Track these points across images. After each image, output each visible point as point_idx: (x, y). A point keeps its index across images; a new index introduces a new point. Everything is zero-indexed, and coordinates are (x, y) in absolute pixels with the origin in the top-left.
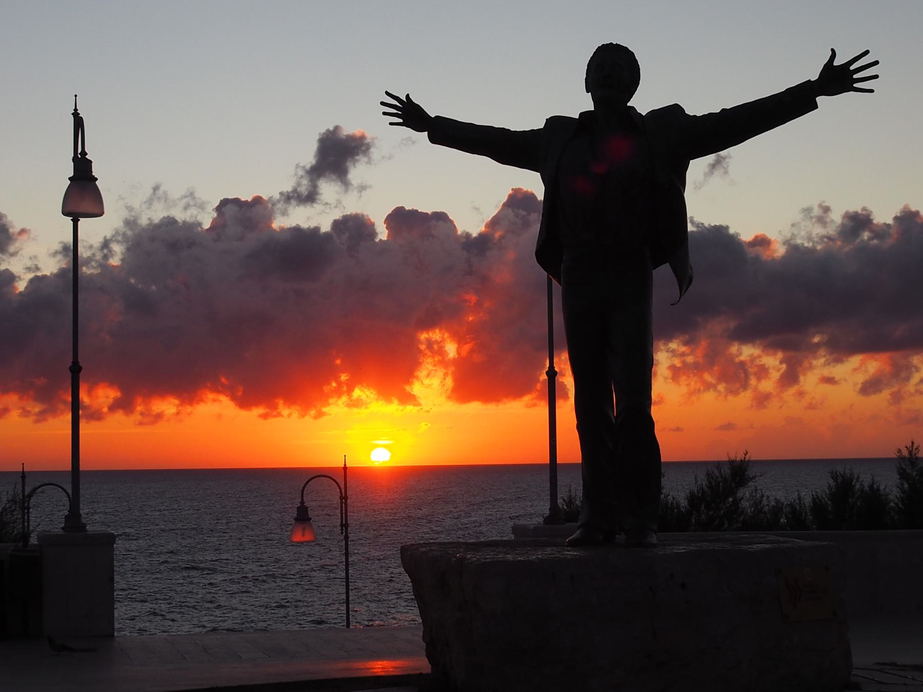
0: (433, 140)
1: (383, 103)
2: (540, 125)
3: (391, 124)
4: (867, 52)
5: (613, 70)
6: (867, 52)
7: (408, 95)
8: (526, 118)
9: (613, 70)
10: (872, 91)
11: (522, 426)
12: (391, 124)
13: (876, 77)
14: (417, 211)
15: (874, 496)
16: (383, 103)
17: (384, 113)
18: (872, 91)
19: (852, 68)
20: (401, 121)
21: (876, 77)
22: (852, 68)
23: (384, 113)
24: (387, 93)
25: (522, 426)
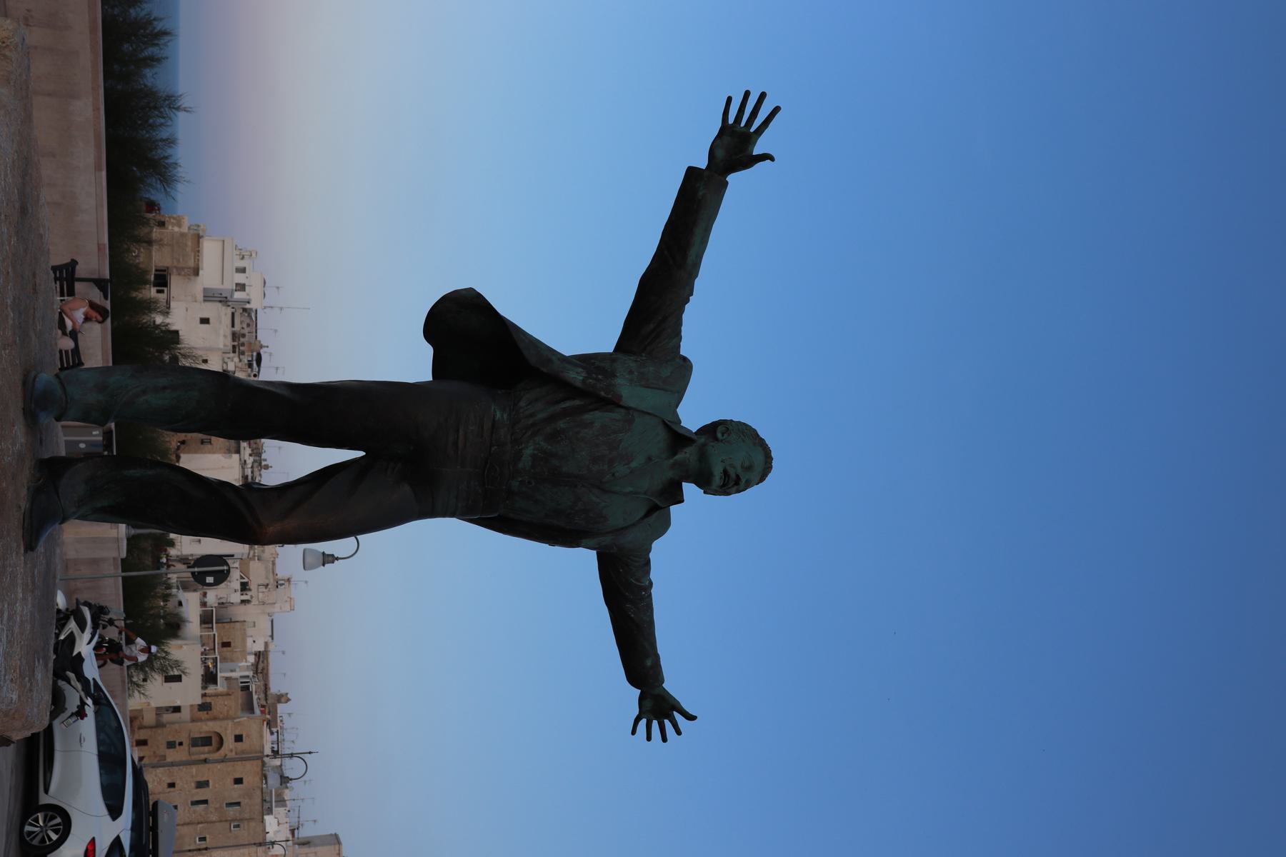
0: (692, 172)
3: (729, 100)
4: (679, 732)
5: (730, 459)
6: (679, 732)
8: (700, 328)
9: (730, 459)
10: (634, 732)
12: (729, 100)
13: (649, 738)
17: (747, 94)
18: (634, 732)
19: (667, 722)
20: (731, 121)
21: (649, 738)
22: (667, 722)
23: (747, 94)
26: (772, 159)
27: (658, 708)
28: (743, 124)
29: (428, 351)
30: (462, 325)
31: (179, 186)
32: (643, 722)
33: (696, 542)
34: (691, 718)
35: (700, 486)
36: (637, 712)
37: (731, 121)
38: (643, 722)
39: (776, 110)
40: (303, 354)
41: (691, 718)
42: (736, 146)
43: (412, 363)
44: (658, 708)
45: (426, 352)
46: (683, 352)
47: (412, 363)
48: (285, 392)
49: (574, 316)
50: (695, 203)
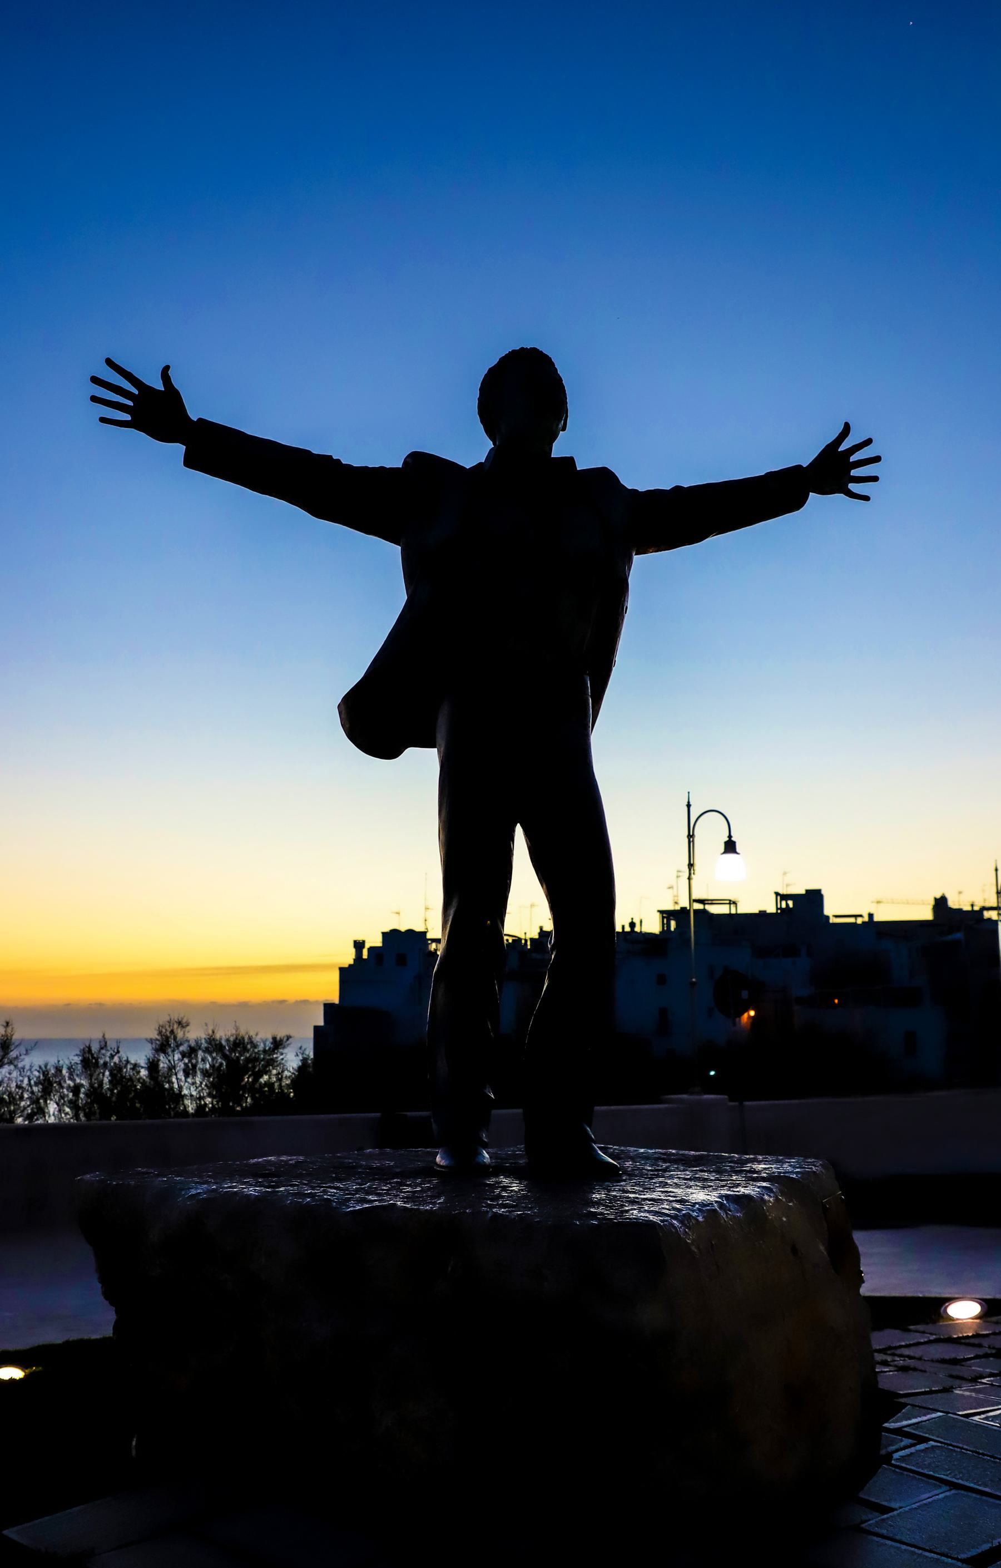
0: (191, 461)
1: (95, 380)
2: (396, 461)
3: (103, 420)
4: (868, 442)
5: (524, 393)
6: (868, 442)
7: (165, 372)
8: (371, 444)
9: (524, 393)
10: (866, 498)
11: (360, 860)
12: (103, 420)
13: (875, 479)
14: (799, 467)
15: (156, 1096)
16: (95, 380)
17: (94, 399)
18: (866, 498)
19: (853, 459)
20: (128, 417)
21: (875, 479)
22: (853, 459)
23: (94, 399)
24: (109, 362)
25: (360, 860)
26: (166, 369)
27: (834, 470)
28: (130, 403)
29: (411, 752)
30: (376, 719)
31: (242, 1032)
32: (853, 487)
33: (631, 432)
34: (847, 429)
35: (554, 437)
36: (840, 496)
37: (128, 417)
38: (853, 487)
39: (109, 362)
40: (416, 900)
41: (847, 429)
42: (155, 411)
43: (421, 767)
44: (834, 470)
45: (411, 753)
46: (352, 962)
47: (421, 767)
48: (443, 815)
49: (355, 595)
50: (227, 454)
